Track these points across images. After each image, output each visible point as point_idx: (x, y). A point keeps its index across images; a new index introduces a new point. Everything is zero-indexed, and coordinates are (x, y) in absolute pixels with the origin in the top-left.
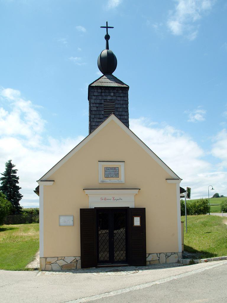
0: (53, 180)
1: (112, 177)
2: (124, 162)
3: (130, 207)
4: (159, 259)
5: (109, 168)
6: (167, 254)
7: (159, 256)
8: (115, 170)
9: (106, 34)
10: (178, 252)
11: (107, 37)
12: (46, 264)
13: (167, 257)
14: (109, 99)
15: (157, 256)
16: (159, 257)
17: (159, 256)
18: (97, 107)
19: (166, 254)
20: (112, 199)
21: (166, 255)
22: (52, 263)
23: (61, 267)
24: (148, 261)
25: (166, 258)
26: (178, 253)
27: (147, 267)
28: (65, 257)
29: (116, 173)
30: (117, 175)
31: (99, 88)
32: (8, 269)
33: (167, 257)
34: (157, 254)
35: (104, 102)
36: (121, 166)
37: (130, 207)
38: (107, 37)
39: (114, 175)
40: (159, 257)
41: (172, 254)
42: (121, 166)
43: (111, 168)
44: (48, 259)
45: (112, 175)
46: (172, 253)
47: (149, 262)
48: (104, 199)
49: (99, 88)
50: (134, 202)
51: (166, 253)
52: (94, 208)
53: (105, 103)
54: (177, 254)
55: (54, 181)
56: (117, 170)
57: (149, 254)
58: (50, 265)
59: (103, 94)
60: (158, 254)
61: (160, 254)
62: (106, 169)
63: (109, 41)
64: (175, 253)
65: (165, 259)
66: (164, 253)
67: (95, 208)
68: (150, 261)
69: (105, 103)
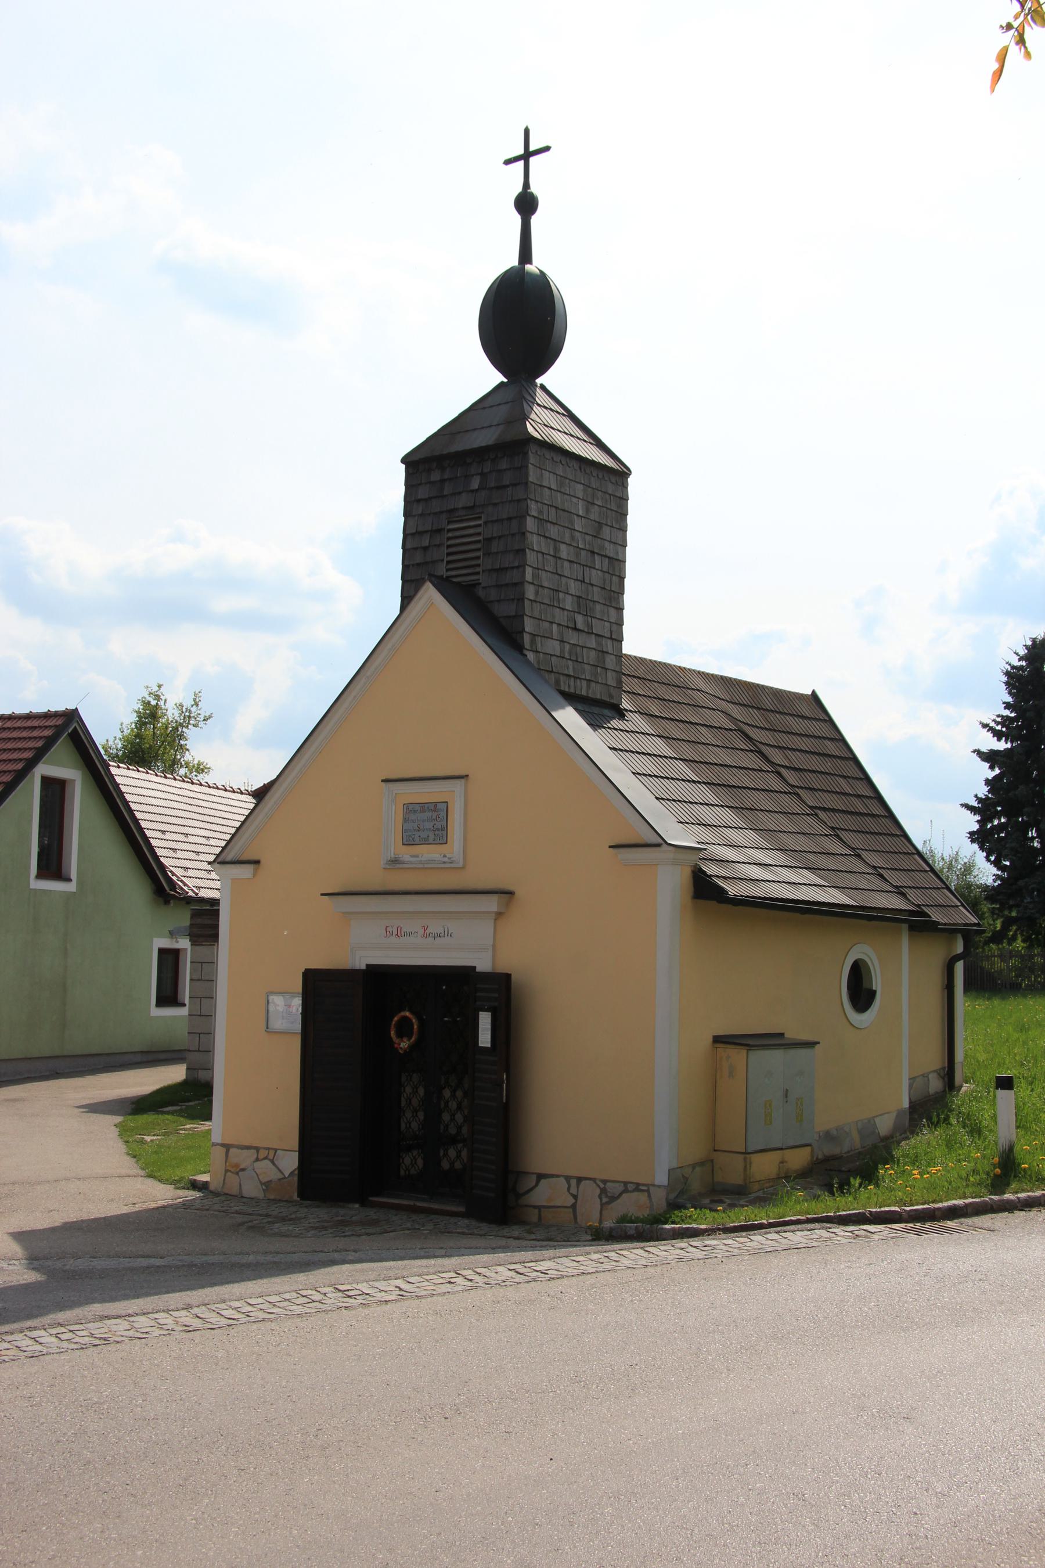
0: (256, 858)
1: (425, 842)
2: (463, 781)
3: (478, 970)
4: (574, 1206)
5: (417, 807)
6: (609, 1184)
7: (574, 1191)
8: (435, 815)
9: (519, 189)
10: (654, 1185)
11: (526, 204)
12: (227, 1171)
13: (605, 1200)
14: (463, 508)
15: (569, 1189)
16: (575, 1197)
17: (574, 1191)
18: (425, 549)
19: (602, 1186)
20: (421, 932)
21: (603, 1191)
22: (242, 1167)
23: (264, 1187)
24: (535, 1207)
25: (602, 1205)
26: (652, 1189)
27: (516, 1231)
28: (276, 1150)
29: (438, 825)
30: (440, 835)
31: (435, 465)
32: (343, 1282)
33: (605, 1200)
34: (568, 1178)
35: (449, 523)
36: (453, 794)
37: (478, 970)
38: (526, 204)
39: (432, 837)
40: (575, 1197)
41: (626, 1191)
42: (453, 794)
43: (425, 807)
44: (232, 1151)
45: (424, 835)
46: (626, 1183)
47: (536, 1211)
48: (395, 932)
49: (435, 465)
50: (490, 953)
51: (605, 1182)
52: (364, 967)
53: (451, 527)
54: (648, 1191)
55: (257, 862)
56: (443, 814)
57: (541, 1177)
58: (237, 1173)
59: (447, 490)
60: (573, 1182)
61: (580, 1180)
62: (410, 809)
63: (535, 220)
64: (638, 1187)
65: (599, 1207)
66: (594, 1180)
67: (367, 965)
68: (539, 1208)
69: (451, 527)
